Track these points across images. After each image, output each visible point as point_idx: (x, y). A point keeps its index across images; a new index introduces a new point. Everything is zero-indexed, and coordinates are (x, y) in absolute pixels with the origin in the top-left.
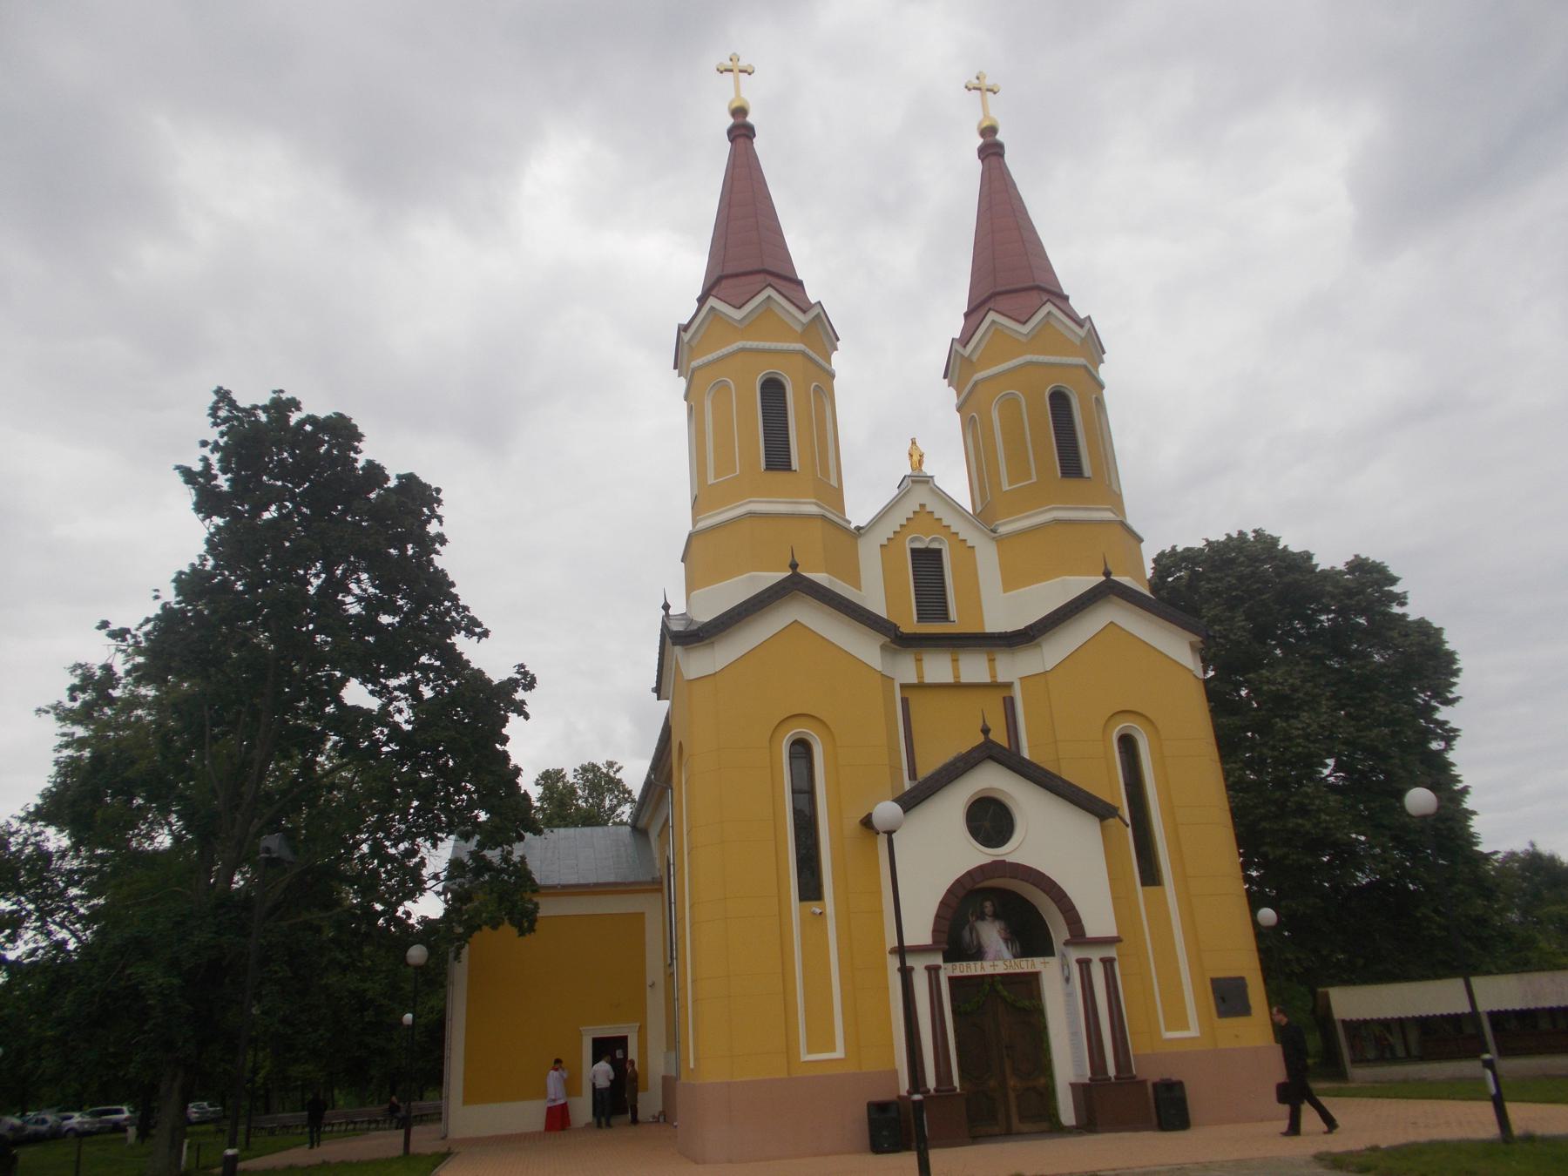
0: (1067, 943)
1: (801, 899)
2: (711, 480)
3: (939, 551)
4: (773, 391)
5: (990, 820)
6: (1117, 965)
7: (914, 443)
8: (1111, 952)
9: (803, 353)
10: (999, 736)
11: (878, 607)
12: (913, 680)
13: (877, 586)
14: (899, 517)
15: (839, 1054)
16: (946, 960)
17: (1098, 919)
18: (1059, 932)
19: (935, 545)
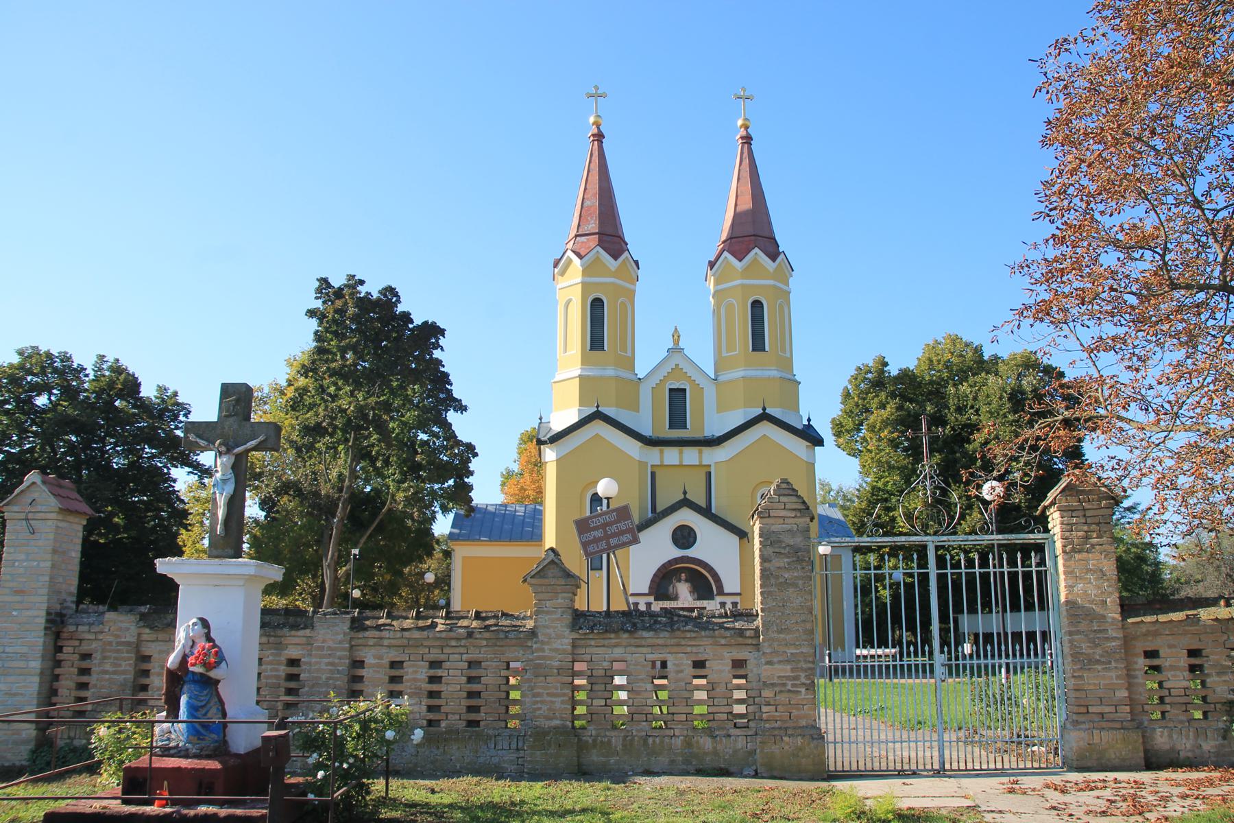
2: (724, 354)
3: (684, 390)
4: (757, 306)
5: (684, 537)
8: (737, 599)
9: (774, 286)
11: (647, 431)
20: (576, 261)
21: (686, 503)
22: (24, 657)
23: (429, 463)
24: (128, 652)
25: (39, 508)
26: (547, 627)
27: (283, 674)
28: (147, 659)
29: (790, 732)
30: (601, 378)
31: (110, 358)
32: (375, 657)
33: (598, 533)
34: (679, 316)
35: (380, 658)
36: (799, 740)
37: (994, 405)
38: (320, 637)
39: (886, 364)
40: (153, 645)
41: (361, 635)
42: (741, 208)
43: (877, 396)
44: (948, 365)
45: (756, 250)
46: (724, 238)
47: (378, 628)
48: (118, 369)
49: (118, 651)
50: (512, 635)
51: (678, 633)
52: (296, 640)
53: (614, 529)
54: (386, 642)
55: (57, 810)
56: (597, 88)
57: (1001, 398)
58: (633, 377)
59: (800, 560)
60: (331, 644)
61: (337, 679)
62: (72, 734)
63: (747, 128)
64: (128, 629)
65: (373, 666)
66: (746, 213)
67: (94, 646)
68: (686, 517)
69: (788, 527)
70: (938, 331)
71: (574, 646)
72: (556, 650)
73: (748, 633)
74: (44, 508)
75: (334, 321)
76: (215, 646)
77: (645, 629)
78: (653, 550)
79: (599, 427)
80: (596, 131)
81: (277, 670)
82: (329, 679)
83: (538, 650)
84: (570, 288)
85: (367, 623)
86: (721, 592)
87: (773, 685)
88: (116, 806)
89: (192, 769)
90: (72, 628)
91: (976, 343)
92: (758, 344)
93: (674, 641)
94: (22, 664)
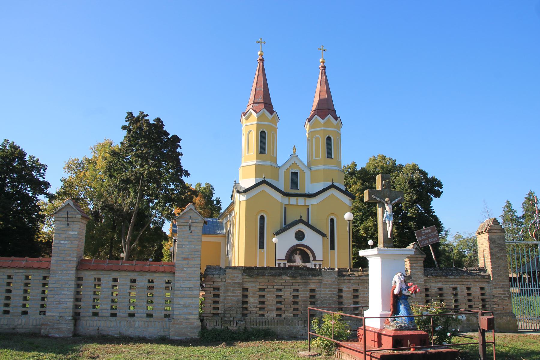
3: (297, 173)
4: (329, 139)
5: (300, 236)
8: (321, 262)
11: (282, 188)
13: (283, 183)
17: (319, 256)
18: (311, 258)
20: (254, 114)
21: (301, 221)
22: (191, 289)
23: (178, 199)
24: (238, 287)
25: (194, 221)
26: (415, 274)
28: (247, 290)
29: (504, 315)
31: (10, 141)
32: (347, 287)
33: (425, 237)
34: (295, 140)
36: (508, 318)
37: (402, 185)
38: (325, 280)
39: (356, 165)
41: (342, 278)
42: (322, 97)
43: (352, 178)
45: (329, 115)
46: (314, 108)
47: (349, 275)
48: (14, 147)
49: (234, 287)
51: (462, 277)
53: (429, 236)
54: (352, 281)
56: (261, 39)
57: (405, 182)
58: (276, 166)
59: (503, 249)
60: (330, 282)
61: (334, 297)
62: (215, 324)
63: (324, 63)
64: (238, 277)
65: (346, 291)
66: (324, 100)
67: (220, 284)
68: (301, 227)
69: (497, 236)
73: (486, 277)
74: (197, 221)
75: (136, 132)
76: (202, 282)
77: (452, 275)
78: (288, 240)
79: (264, 187)
80: (261, 58)
81: (306, 294)
82: (330, 297)
84: (249, 126)
86: (315, 259)
87: (497, 297)
88: (391, 352)
90: (211, 276)
91: (394, 159)
92: (329, 156)
93: (459, 280)
94: (190, 293)
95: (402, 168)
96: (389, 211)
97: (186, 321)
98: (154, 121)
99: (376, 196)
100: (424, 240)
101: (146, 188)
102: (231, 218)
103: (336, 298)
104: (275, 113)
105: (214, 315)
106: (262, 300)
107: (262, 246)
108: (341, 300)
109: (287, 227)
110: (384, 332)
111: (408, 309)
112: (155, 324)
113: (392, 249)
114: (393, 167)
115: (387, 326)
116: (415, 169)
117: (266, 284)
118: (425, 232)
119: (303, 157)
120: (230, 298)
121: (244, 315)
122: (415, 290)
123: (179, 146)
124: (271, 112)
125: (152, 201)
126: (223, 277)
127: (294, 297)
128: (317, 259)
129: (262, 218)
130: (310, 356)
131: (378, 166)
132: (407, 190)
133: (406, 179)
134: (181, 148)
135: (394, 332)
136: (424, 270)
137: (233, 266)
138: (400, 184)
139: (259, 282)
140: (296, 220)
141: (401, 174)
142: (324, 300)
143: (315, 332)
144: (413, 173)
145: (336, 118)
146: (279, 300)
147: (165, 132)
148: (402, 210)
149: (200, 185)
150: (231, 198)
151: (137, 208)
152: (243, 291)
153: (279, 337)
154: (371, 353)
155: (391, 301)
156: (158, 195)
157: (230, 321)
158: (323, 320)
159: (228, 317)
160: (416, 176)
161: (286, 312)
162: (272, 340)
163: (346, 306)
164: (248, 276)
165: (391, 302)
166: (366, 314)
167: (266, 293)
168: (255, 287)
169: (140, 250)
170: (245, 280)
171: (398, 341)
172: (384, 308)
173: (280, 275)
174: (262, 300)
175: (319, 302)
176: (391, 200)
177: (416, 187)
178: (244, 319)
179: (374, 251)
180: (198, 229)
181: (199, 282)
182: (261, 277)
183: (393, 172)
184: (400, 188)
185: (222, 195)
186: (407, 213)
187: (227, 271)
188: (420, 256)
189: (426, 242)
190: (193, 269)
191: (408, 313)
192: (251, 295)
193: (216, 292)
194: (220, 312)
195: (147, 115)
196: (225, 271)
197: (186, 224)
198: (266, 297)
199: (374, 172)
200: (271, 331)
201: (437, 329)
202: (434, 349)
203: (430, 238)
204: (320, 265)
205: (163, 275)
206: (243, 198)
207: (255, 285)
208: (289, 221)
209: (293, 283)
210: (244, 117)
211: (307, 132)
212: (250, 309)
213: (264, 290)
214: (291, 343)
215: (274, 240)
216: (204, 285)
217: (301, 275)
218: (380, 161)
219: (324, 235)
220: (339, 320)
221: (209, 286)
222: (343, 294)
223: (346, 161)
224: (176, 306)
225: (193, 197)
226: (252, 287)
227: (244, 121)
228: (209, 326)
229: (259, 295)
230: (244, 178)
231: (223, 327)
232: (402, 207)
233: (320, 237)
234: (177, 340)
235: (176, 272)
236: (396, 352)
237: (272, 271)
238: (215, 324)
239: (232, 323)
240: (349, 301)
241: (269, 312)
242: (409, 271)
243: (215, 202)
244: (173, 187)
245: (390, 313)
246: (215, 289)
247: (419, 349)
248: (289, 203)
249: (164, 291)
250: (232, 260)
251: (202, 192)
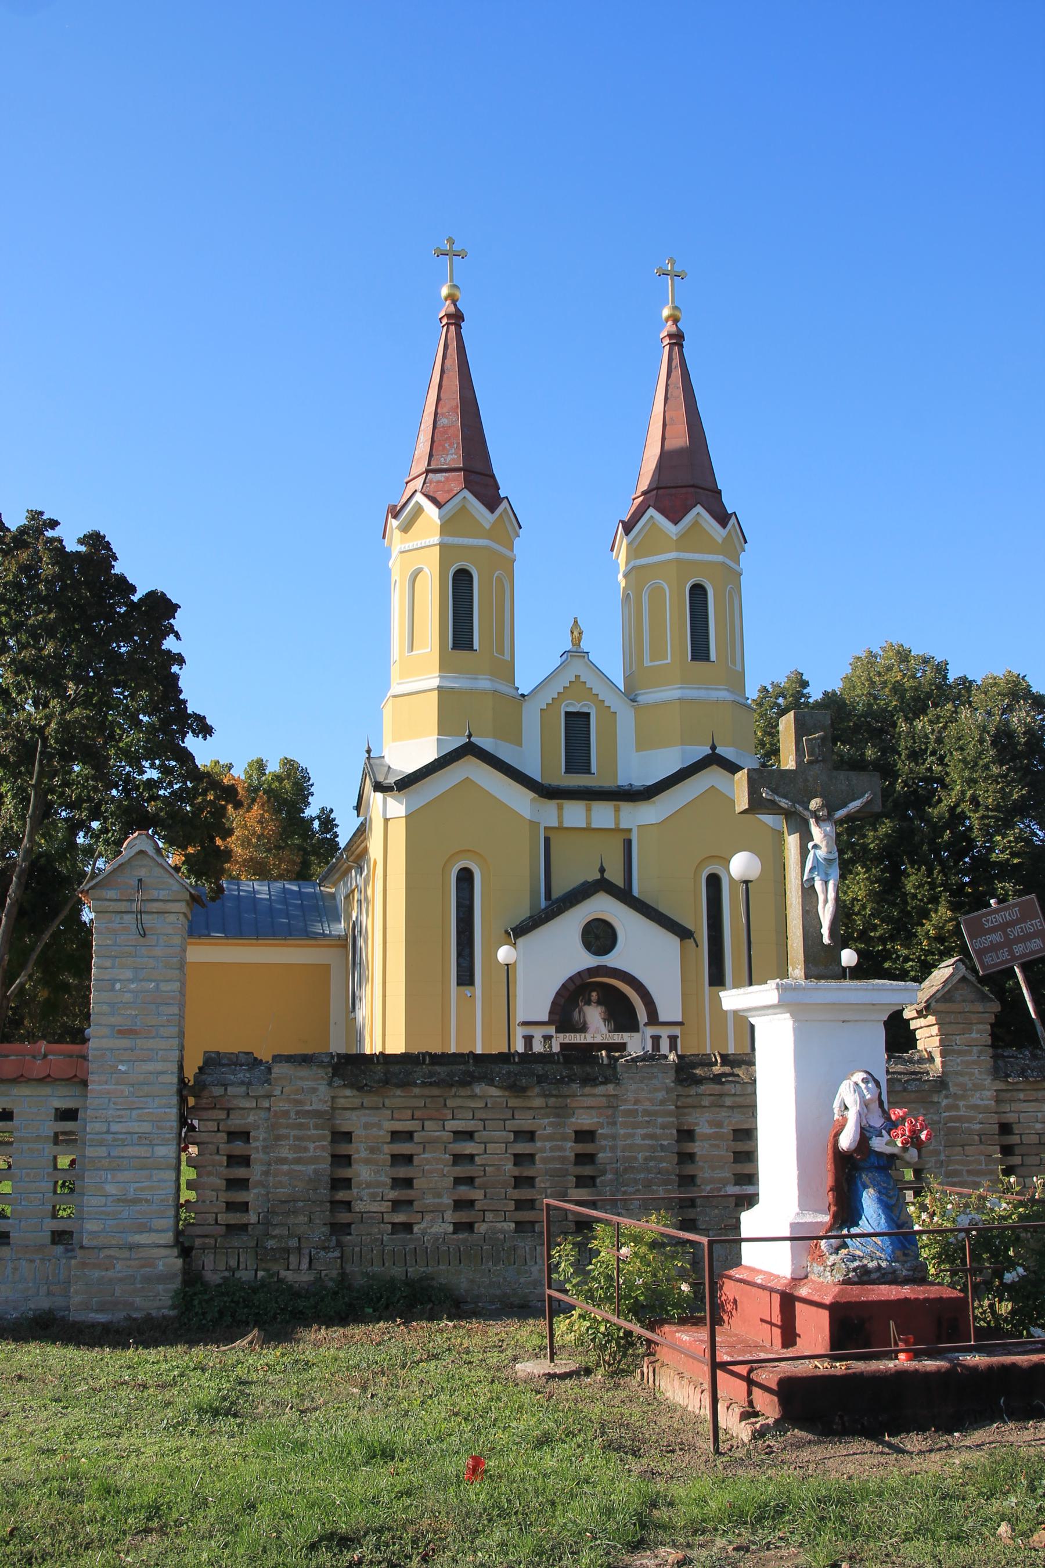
0: (646, 1025)
1: (458, 984)
2: (647, 663)
3: (588, 715)
4: (698, 592)
5: (600, 937)
6: (679, 1041)
7: (576, 622)
8: (676, 1031)
10: (615, 876)
11: (534, 771)
12: (555, 824)
13: (535, 751)
14: (558, 687)
15: (669, 661)
16: (557, 1032)
17: (669, 1008)
18: (642, 1016)
19: (585, 710)
20: (431, 511)
21: (602, 885)
22: (145, 1139)
23: (172, 815)
24: (316, 1127)
25: (155, 894)
26: (957, 1073)
27: (571, 1155)
30: (471, 692)
32: (712, 1124)
33: (997, 937)
34: (578, 600)
35: (720, 1125)
37: (971, 751)
38: (631, 1096)
39: (805, 684)
40: (354, 1115)
44: (897, 689)
45: (699, 509)
46: (644, 485)
47: (717, 1079)
49: (301, 1127)
50: (912, 1087)
52: (589, 1102)
53: (1015, 932)
54: (728, 1101)
55: (879, 1371)
56: (452, 242)
57: (981, 741)
58: (513, 692)
62: (233, 1263)
63: (676, 321)
64: (314, 1090)
65: (708, 1137)
66: (679, 452)
67: (251, 1119)
68: (603, 907)
70: (875, 638)
71: (998, 1101)
72: (975, 1107)
74: (163, 894)
78: (556, 955)
79: (472, 769)
81: (561, 1149)
82: (646, 1159)
83: (949, 1108)
84: (416, 553)
85: (698, 1071)
86: (653, 1019)
88: (823, 1367)
89: (926, 1300)
90: (218, 1091)
91: (939, 659)
92: (700, 651)
94: (142, 1151)
95: (968, 689)
96: (823, 845)
97: (126, 1254)
98: (81, 541)
99: (775, 791)
100: (994, 948)
101: (56, 781)
102: (361, 881)
103: (668, 1163)
104: (505, 503)
105: (231, 1229)
106: (402, 1172)
107: (466, 977)
108: (689, 1170)
109: (553, 907)
110: (803, 1292)
111: (892, 1208)
112: (15, 1269)
113: (833, 983)
114: (939, 687)
115: (817, 1268)
116: (1017, 691)
117: (417, 1114)
118: (999, 918)
119: (609, 658)
120: (287, 1166)
121: (339, 1229)
122: (915, 1133)
123: (171, 630)
124: (491, 498)
125: (82, 825)
126: (260, 1091)
127: (519, 1159)
128: (662, 1019)
129: (465, 877)
130: (551, 1376)
131: (885, 682)
132: (986, 767)
133: (984, 729)
134: (178, 637)
135: (837, 1289)
136: (995, 1057)
137: (368, 1052)
138: (961, 749)
139: (393, 1110)
140: (586, 883)
141: (965, 713)
142: (626, 1170)
143: (565, 1291)
144: (1009, 709)
145: (723, 517)
146: (462, 1171)
147: (122, 580)
148: (971, 842)
149: (260, 766)
150: (358, 808)
151: (28, 851)
152: (333, 1141)
153: (459, 1307)
154: (750, 1371)
155: (827, 1178)
156: (99, 805)
157: (287, 1251)
158: (594, 1244)
159: (279, 1238)
160: (1020, 718)
161: (489, 1216)
162: (431, 1319)
163: (706, 1190)
164: (351, 1086)
165: (829, 1180)
166: (750, 1222)
167: (420, 1149)
168: (379, 1126)
169: (47, 1000)
170: (341, 1102)
171: (851, 1326)
172: (804, 1204)
173: (467, 1081)
174: (402, 1172)
175: (610, 1176)
176: (831, 807)
177: (1020, 756)
178: (340, 1245)
179: (766, 993)
180: (172, 920)
181: (173, 1112)
182: (398, 1092)
183: (936, 705)
184: (964, 761)
185: (331, 795)
186: (991, 850)
187: (278, 1070)
188: (979, 1007)
189: (1004, 955)
190: (151, 1067)
191: (890, 1219)
192: (364, 1154)
193: (238, 1148)
194: (253, 1218)
195: (54, 524)
196: (269, 1070)
197: (123, 906)
198: (416, 1160)
199: (870, 705)
200: (434, 1283)
201: (1009, 1277)
202: (989, 1351)
203: (1019, 940)
204: (673, 1039)
205: (47, 1090)
206: (397, 807)
207: (376, 1120)
208: (561, 887)
209: (513, 1109)
210: (394, 523)
211: (622, 568)
212: (359, 1206)
213: (409, 1136)
214: (496, 1329)
215: (504, 954)
216: (195, 1122)
217: (541, 1080)
218: (889, 669)
219: (683, 933)
220: (653, 1245)
221: (212, 1126)
222: (698, 1148)
223: (763, 670)
224: (92, 1202)
225: (224, 808)
226: (366, 1126)
227: (397, 534)
228: (213, 1269)
229: (393, 1156)
230: (397, 737)
231: (260, 1274)
232: (970, 829)
233: (674, 941)
234: (93, 1325)
235: (91, 1078)
236: (840, 1368)
237: (438, 1068)
238: (233, 1263)
239: (293, 1259)
240: (719, 1174)
241: (428, 1217)
242: (938, 1060)
243: (316, 824)
244: (153, 774)
245: (826, 1218)
246: (233, 1136)
247: (931, 1355)
248: (561, 822)
249: (49, 1149)
250: (364, 1025)
251: (266, 792)
